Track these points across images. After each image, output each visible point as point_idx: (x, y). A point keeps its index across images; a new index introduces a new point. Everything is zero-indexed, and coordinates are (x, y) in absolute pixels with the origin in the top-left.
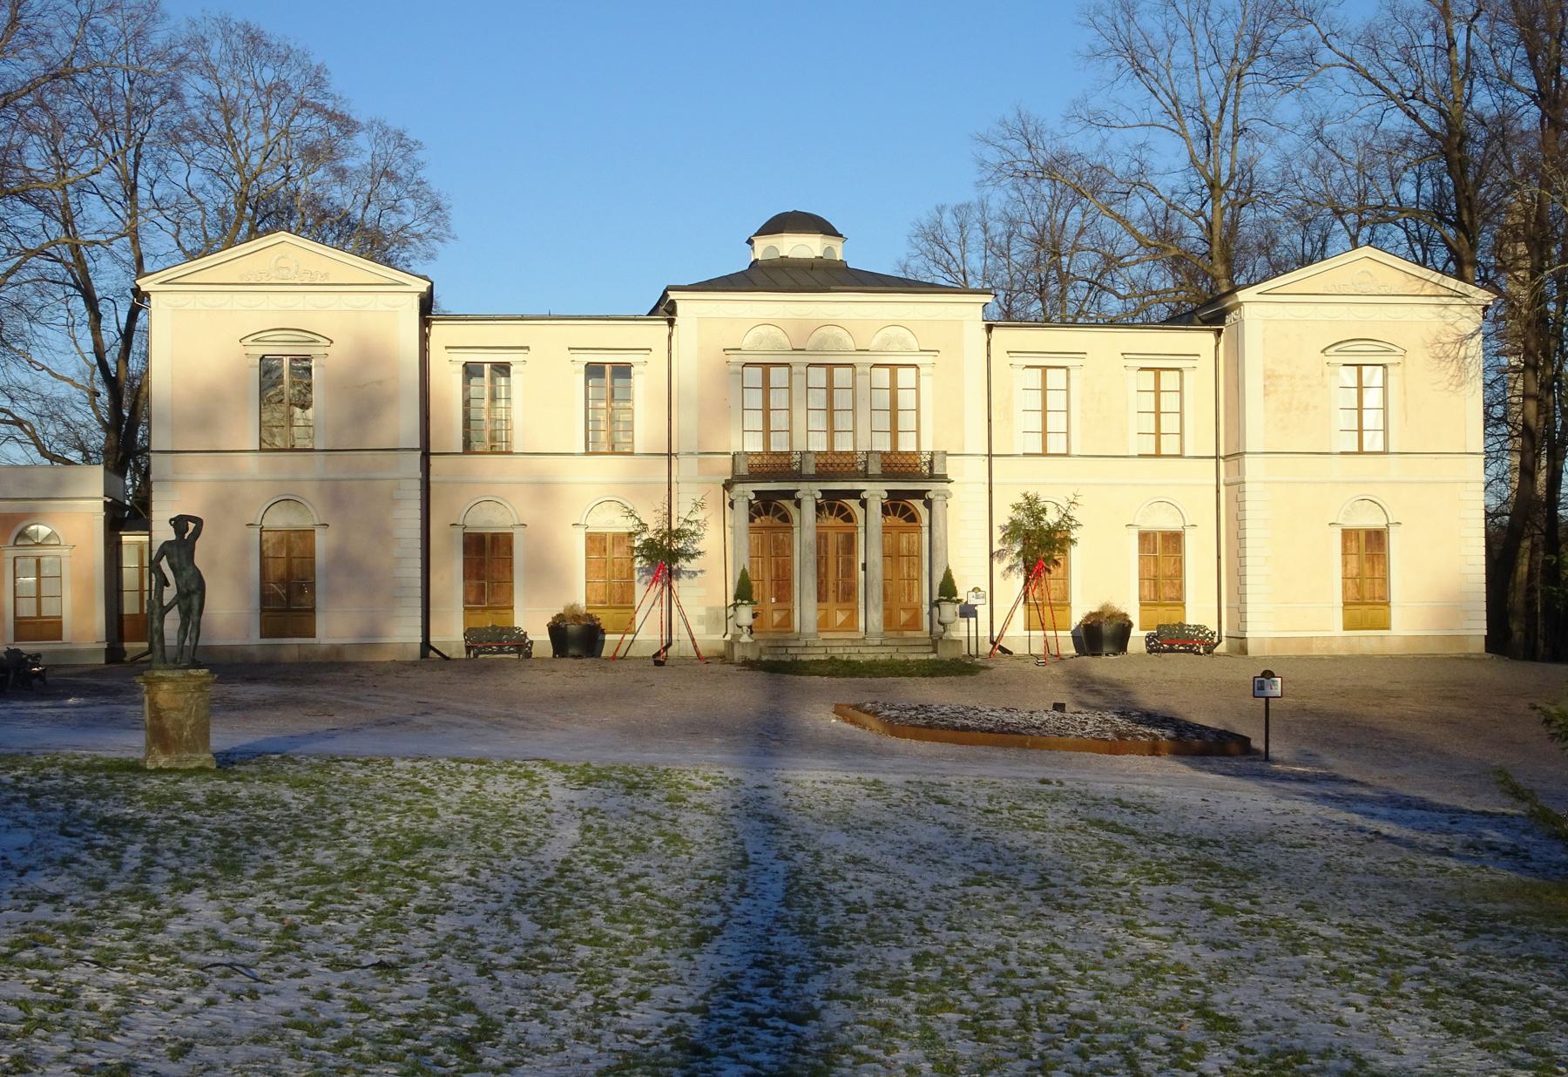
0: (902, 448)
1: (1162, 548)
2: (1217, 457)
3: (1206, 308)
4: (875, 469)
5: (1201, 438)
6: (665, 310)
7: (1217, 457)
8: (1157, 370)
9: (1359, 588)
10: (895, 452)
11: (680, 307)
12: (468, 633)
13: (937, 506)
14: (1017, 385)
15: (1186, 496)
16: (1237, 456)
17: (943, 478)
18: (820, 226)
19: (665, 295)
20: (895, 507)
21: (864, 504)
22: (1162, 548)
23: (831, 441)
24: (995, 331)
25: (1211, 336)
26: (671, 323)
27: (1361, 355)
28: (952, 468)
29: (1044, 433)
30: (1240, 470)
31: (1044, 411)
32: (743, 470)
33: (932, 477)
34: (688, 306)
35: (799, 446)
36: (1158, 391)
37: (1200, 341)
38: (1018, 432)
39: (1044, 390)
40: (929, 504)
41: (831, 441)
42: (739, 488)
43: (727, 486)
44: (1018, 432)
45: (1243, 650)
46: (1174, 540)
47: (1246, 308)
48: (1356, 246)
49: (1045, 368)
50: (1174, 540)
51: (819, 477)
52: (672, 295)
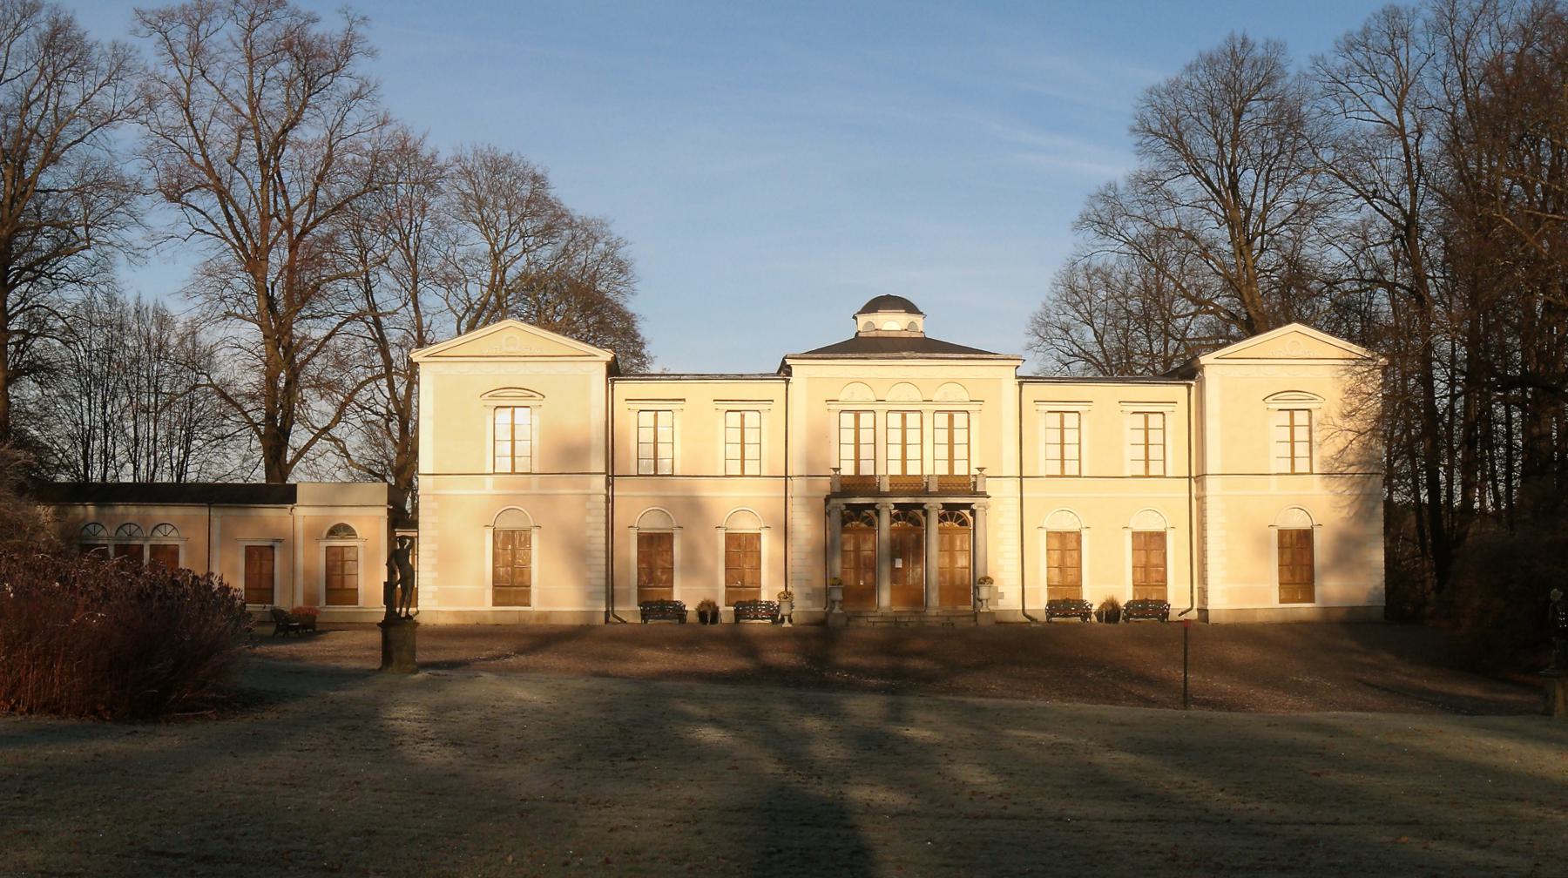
0: (909, 472)
1: (1150, 545)
2: (1190, 477)
3: (1188, 373)
4: (933, 488)
5: (1177, 463)
6: (785, 371)
7: (1190, 477)
8: (1146, 413)
9: (1147, 575)
10: (951, 474)
11: (794, 369)
12: (1050, 604)
13: (979, 515)
14: (1042, 427)
15: (1163, 508)
16: (1201, 478)
17: (984, 495)
18: (911, 308)
19: (784, 362)
20: (951, 516)
21: (926, 513)
22: (1150, 545)
23: (951, 467)
24: (1025, 387)
25: (1184, 388)
26: (787, 382)
27: (1291, 403)
28: (990, 486)
29: (1147, 460)
30: (1202, 487)
31: (1147, 445)
32: (837, 489)
33: (975, 494)
34: (800, 370)
35: (928, 471)
36: (1292, 426)
37: (1177, 392)
38: (1042, 459)
39: (1147, 429)
40: (973, 513)
41: (951, 467)
42: (834, 501)
43: (827, 500)
44: (1042, 459)
45: (1207, 620)
46: (1160, 537)
47: (1207, 370)
48: (459, 333)
49: (1292, 411)
50: (1160, 537)
51: (942, 493)
52: (789, 362)
